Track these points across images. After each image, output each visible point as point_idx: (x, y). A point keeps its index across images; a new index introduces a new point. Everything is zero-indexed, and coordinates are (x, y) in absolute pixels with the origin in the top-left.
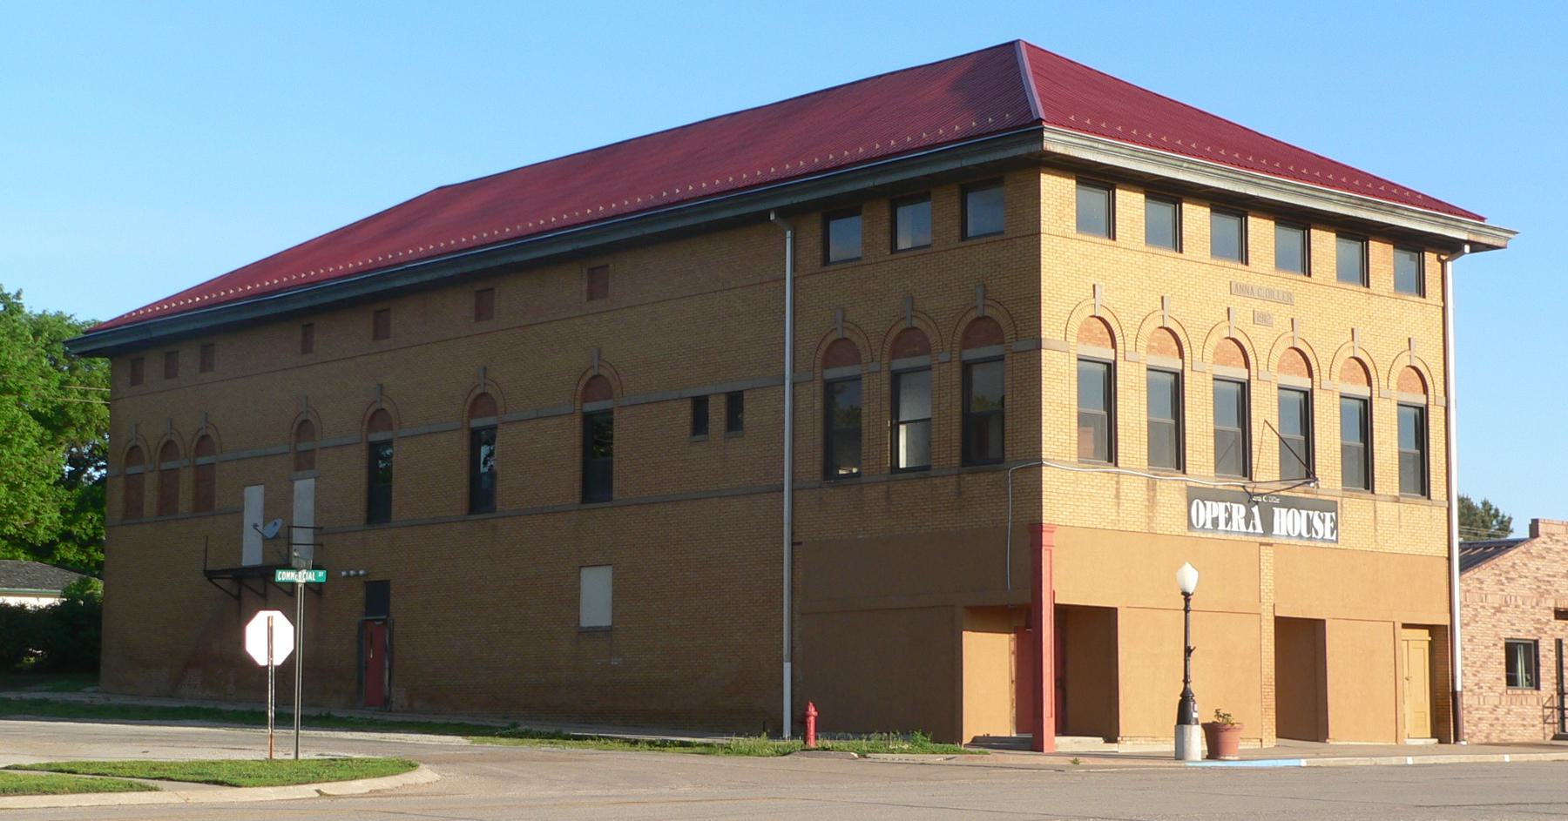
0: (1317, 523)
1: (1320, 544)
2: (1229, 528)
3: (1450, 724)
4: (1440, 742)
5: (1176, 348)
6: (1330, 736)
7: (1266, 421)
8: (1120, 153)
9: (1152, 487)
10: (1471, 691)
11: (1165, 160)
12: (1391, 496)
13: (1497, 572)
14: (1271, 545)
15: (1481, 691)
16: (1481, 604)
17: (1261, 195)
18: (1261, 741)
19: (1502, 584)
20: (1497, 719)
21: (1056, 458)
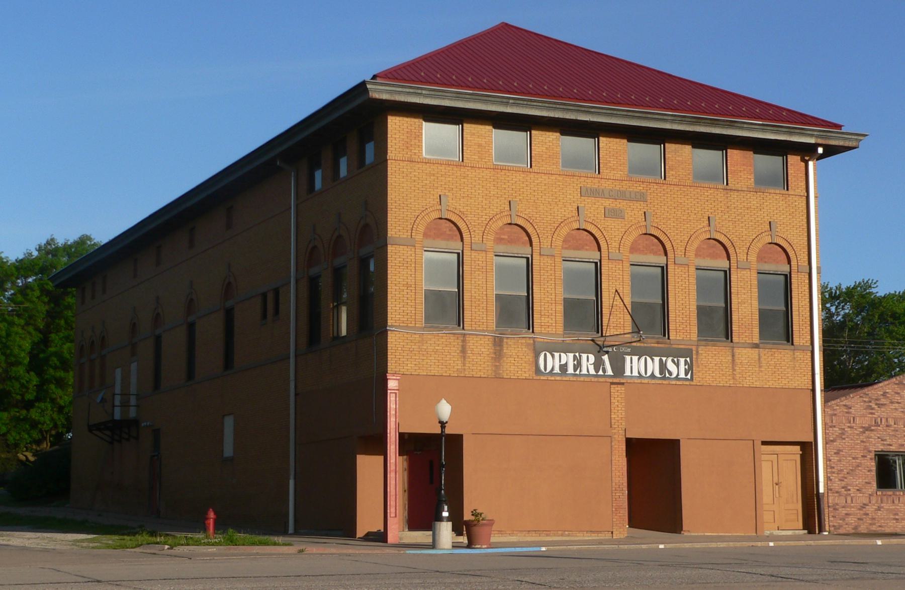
0: (671, 366)
1: (674, 382)
2: (578, 372)
3: (815, 519)
4: (809, 533)
5: (527, 238)
6: (684, 528)
7: (616, 291)
8: (446, 96)
9: (498, 343)
10: (837, 492)
11: (490, 99)
12: (749, 343)
13: (867, 400)
14: (623, 384)
15: (849, 492)
16: (849, 425)
17: (592, 120)
18: (612, 533)
19: (873, 409)
20: (867, 514)
21: (401, 324)
